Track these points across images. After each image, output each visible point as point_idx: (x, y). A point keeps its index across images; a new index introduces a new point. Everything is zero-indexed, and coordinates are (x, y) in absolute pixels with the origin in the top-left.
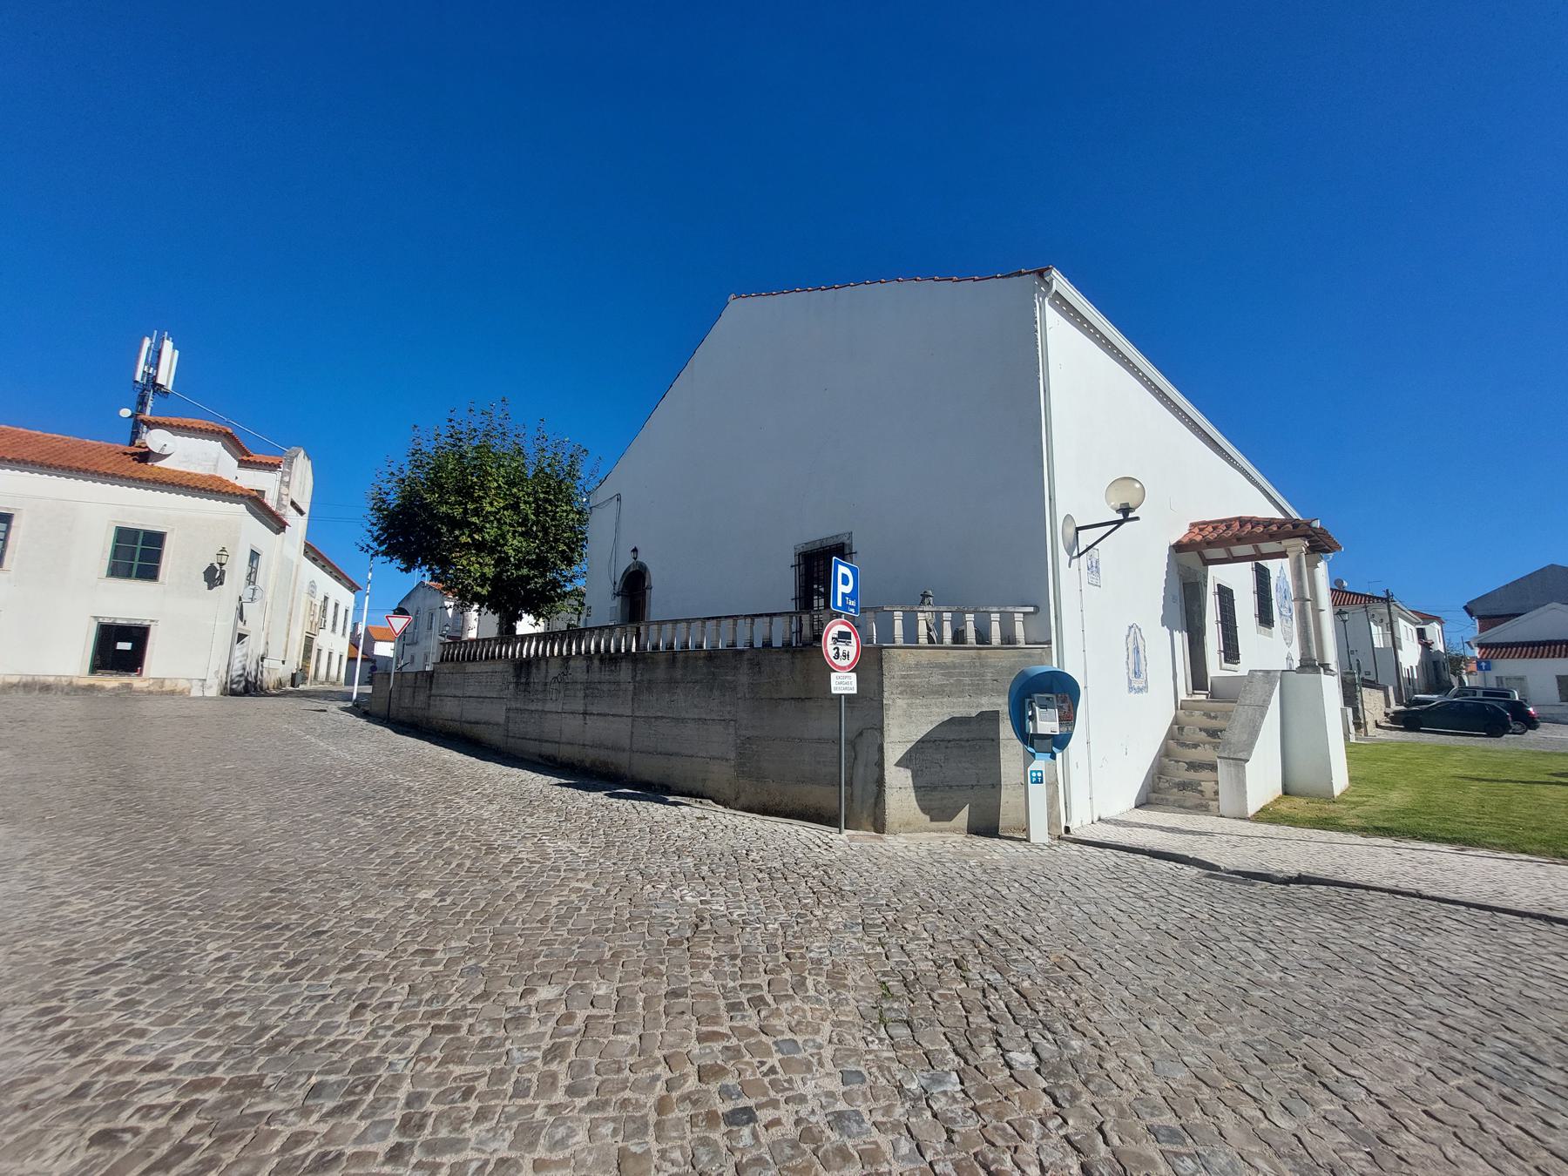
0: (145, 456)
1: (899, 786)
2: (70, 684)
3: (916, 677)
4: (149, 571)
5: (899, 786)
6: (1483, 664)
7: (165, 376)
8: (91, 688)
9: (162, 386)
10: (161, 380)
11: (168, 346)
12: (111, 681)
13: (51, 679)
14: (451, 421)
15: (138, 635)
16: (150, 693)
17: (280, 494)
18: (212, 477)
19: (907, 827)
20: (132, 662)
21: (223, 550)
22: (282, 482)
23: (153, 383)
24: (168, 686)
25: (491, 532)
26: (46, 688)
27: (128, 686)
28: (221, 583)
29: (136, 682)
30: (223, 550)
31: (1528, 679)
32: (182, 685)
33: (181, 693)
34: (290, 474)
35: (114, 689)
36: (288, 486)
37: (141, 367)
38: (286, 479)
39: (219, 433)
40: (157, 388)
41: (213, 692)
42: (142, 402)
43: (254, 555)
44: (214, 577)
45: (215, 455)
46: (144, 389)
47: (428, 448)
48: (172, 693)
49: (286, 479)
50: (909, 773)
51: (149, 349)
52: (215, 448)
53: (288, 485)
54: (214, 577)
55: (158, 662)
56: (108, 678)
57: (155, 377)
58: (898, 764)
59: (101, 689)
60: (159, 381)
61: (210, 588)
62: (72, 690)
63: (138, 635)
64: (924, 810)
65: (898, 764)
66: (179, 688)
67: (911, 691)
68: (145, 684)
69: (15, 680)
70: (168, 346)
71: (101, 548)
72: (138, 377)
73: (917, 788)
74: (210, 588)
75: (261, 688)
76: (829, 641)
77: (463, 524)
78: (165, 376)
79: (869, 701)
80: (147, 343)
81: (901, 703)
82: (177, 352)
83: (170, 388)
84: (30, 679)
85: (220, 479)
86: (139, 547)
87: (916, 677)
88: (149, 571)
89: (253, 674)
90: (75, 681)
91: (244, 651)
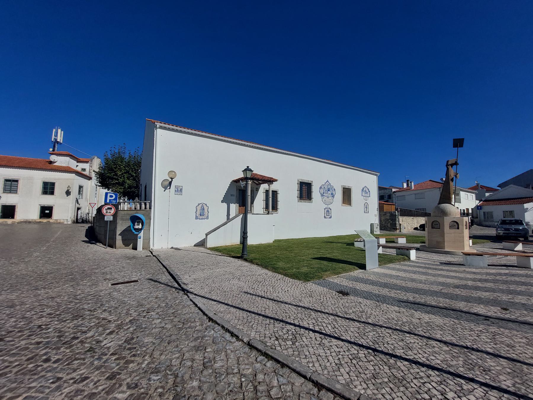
0: (51, 162)
1: (119, 239)
2: (35, 221)
3: (123, 217)
4: (52, 193)
5: (119, 239)
6: (479, 207)
7: (60, 139)
8: (40, 222)
9: (59, 142)
10: (58, 140)
11: (59, 131)
12: (45, 220)
13: (31, 220)
14: (111, 150)
15: (50, 208)
16: (54, 223)
17: (90, 169)
18: (67, 167)
19: (120, 248)
20: (49, 216)
21: (69, 186)
22: (90, 166)
23: (56, 142)
24: (59, 221)
25: (121, 180)
26: (30, 222)
27: (49, 221)
28: (70, 195)
29: (51, 221)
30: (69, 186)
31: (515, 212)
32: (62, 221)
33: (62, 223)
34: (92, 163)
35: (45, 222)
36: (91, 167)
37: (53, 137)
38: (91, 165)
39: (68, 155)
40: (58, 142)
41: (70, 223)
42: (54, 147)
43: (81, 187)
44: (68, 193)
45: (68, 161)
46: (55, 143)
47: (110, 156)
48: (60, 223)
49: (91, 165)
50: (121, 237)
51: (55, 132)
52: (68, 159)
53: (91, 167)
54: (68, 193)
55: (56, 215)
56: (44, 220)
57: (57, 140)
58: (119, 235)
59: (43, 222)
60: (58, 141)
61: (67, 196)
62: (36, 222)
63: (50, 208)
64: (124, 244)
65: (119, 235)
66: (61, 222)
67: (122, 220)
68: (53, 221)
69: (23, 220)
70: (59, 131)
71: (39, 187)
72: (53, 140)
73: (122, 240)
74: (67, 196)
75: (89, 222)
76: (104, 209)
77: (112, 179)
78: (60, 139)
79: (114, 222)
80: (54, 130)
81: (120, 222)
82: (63, 132)
83: (62, 142)
84: (26, 220)
85: (69, 167)
86: (49, 186)
87: (123, 217)
88: (52, 193)
89: (85, 218)
90: (36, 220)
91: (81, 212)
